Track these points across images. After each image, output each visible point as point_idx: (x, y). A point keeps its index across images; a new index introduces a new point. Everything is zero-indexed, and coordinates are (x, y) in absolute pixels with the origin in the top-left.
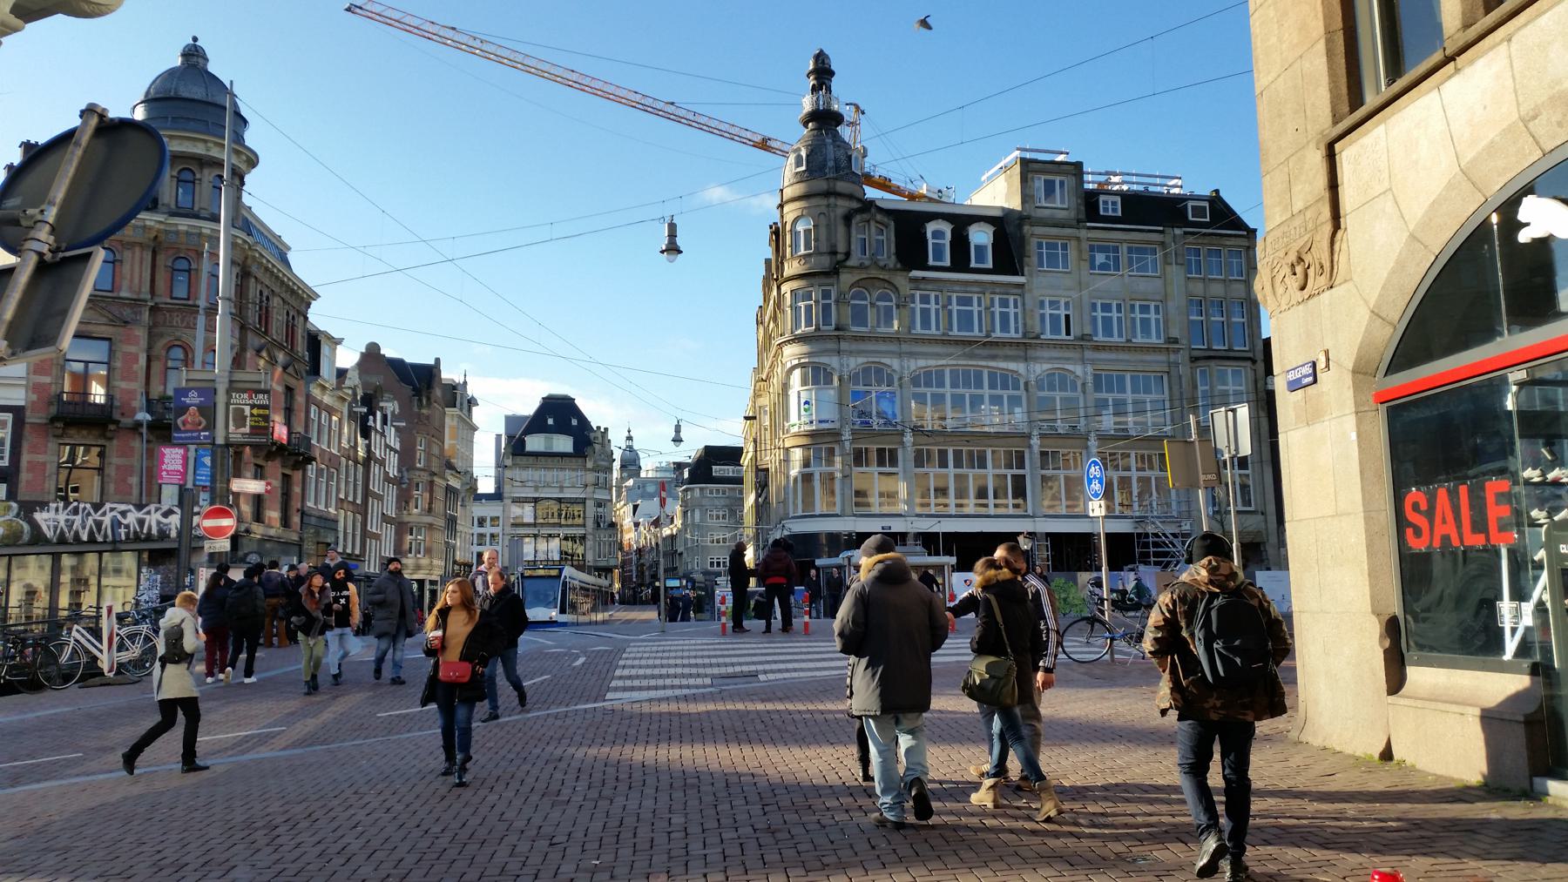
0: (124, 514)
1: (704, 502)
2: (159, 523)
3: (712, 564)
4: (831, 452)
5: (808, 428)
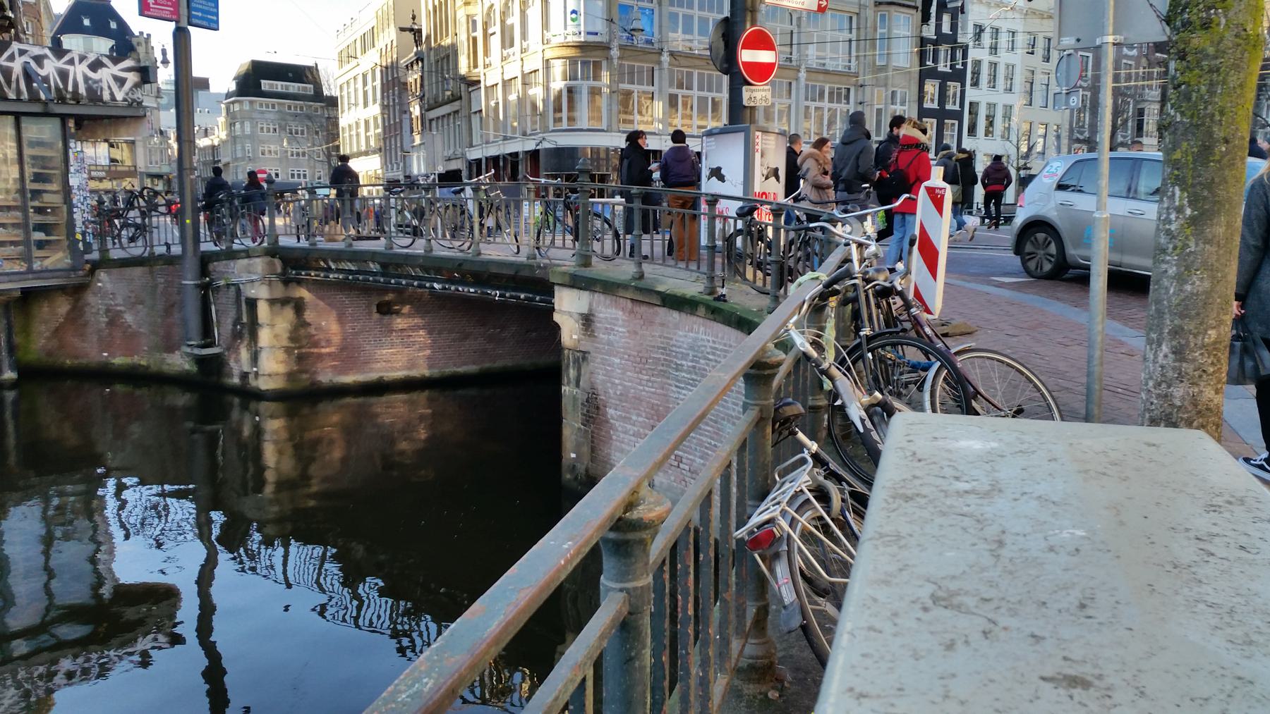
0: (39, 60)
1: (255, 115)
2: (86, 79)
3: (293, 176)
4: (597, 66)
5: (576, 39)
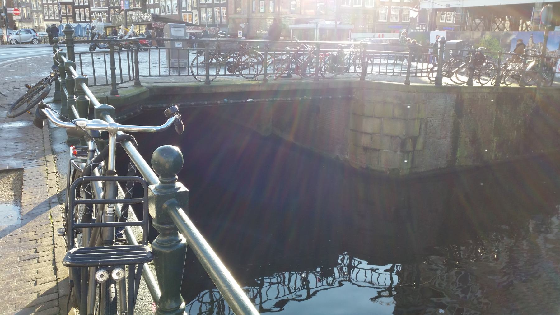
0: (142, 16)
